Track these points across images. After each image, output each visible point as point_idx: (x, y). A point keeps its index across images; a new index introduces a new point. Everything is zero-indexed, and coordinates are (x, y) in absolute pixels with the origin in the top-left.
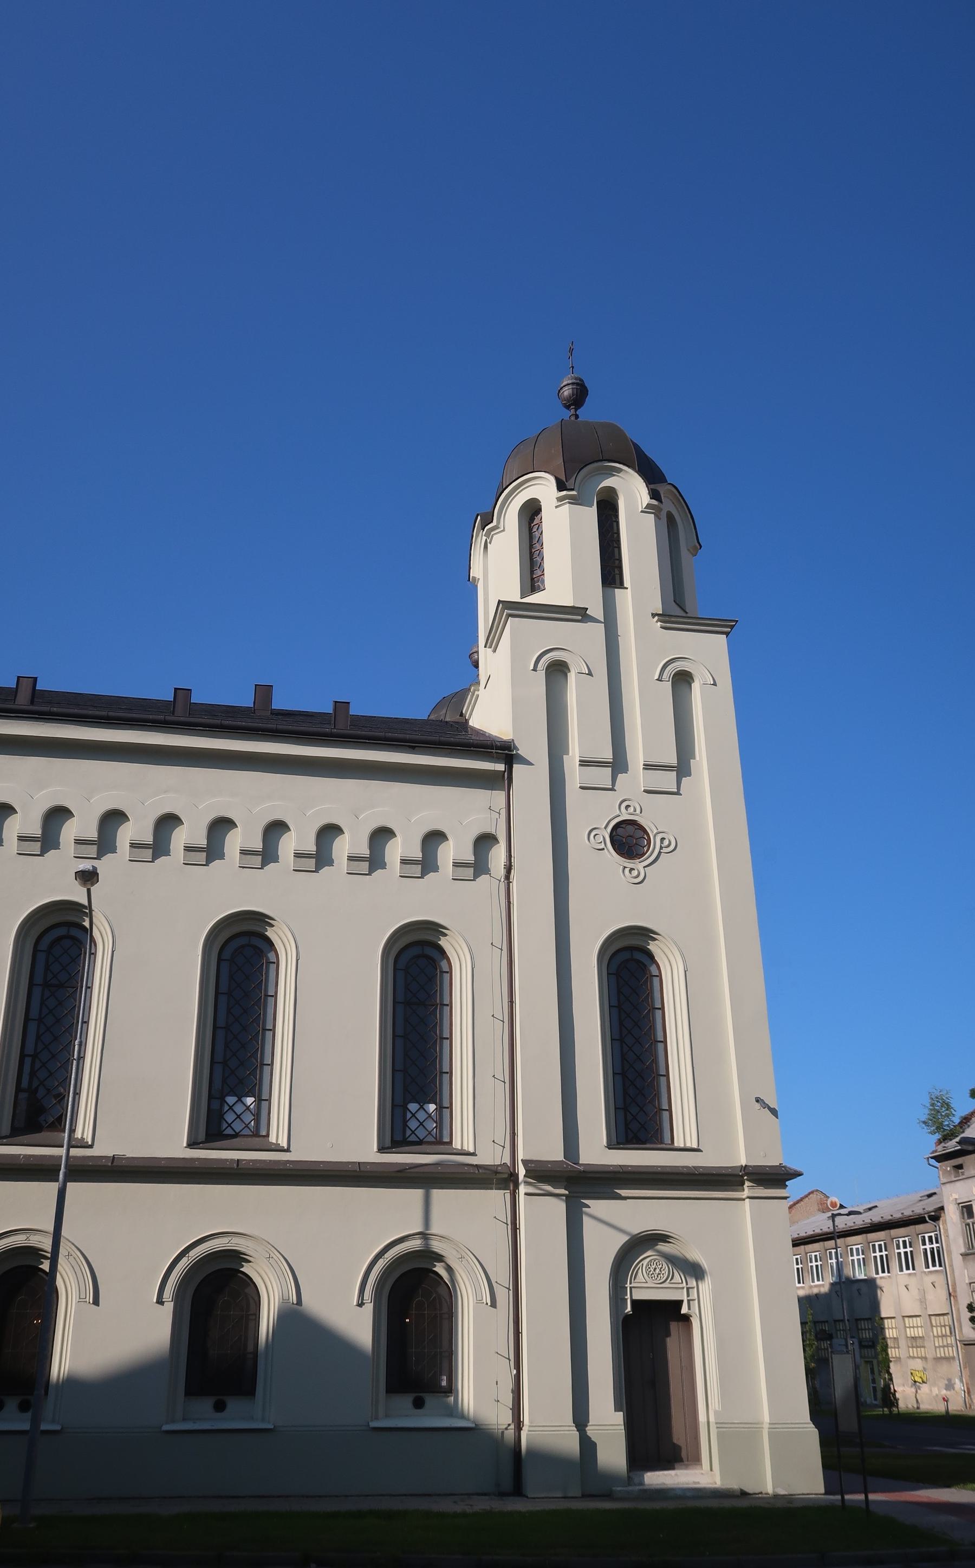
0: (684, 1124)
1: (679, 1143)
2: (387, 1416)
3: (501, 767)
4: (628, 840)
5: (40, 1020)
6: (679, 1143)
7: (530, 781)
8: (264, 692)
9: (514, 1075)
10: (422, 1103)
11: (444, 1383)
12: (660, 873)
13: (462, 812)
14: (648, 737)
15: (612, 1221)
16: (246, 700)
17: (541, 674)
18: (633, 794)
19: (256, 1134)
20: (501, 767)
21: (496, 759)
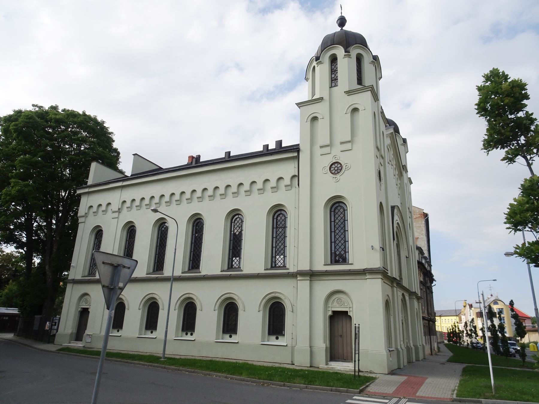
0: (351, 256)
1: (350, 263)
2: (268, 341)
3: (295, 154)
4: (336, 168)
5: (335, 242)
6: (350, 263)
7: (304, 157)
8: (279, 143)
9: (306, 246)
10: (236, 257)
11: (7, 318)
12: (343, 177)
13: (287, 170)
14: (343, 132)
15: (324, 287)
16: (261, 149)
17: (309, 123)
18: (337, 153)
19: (239, 267)
20: (295, 154)
21: (294, 152)
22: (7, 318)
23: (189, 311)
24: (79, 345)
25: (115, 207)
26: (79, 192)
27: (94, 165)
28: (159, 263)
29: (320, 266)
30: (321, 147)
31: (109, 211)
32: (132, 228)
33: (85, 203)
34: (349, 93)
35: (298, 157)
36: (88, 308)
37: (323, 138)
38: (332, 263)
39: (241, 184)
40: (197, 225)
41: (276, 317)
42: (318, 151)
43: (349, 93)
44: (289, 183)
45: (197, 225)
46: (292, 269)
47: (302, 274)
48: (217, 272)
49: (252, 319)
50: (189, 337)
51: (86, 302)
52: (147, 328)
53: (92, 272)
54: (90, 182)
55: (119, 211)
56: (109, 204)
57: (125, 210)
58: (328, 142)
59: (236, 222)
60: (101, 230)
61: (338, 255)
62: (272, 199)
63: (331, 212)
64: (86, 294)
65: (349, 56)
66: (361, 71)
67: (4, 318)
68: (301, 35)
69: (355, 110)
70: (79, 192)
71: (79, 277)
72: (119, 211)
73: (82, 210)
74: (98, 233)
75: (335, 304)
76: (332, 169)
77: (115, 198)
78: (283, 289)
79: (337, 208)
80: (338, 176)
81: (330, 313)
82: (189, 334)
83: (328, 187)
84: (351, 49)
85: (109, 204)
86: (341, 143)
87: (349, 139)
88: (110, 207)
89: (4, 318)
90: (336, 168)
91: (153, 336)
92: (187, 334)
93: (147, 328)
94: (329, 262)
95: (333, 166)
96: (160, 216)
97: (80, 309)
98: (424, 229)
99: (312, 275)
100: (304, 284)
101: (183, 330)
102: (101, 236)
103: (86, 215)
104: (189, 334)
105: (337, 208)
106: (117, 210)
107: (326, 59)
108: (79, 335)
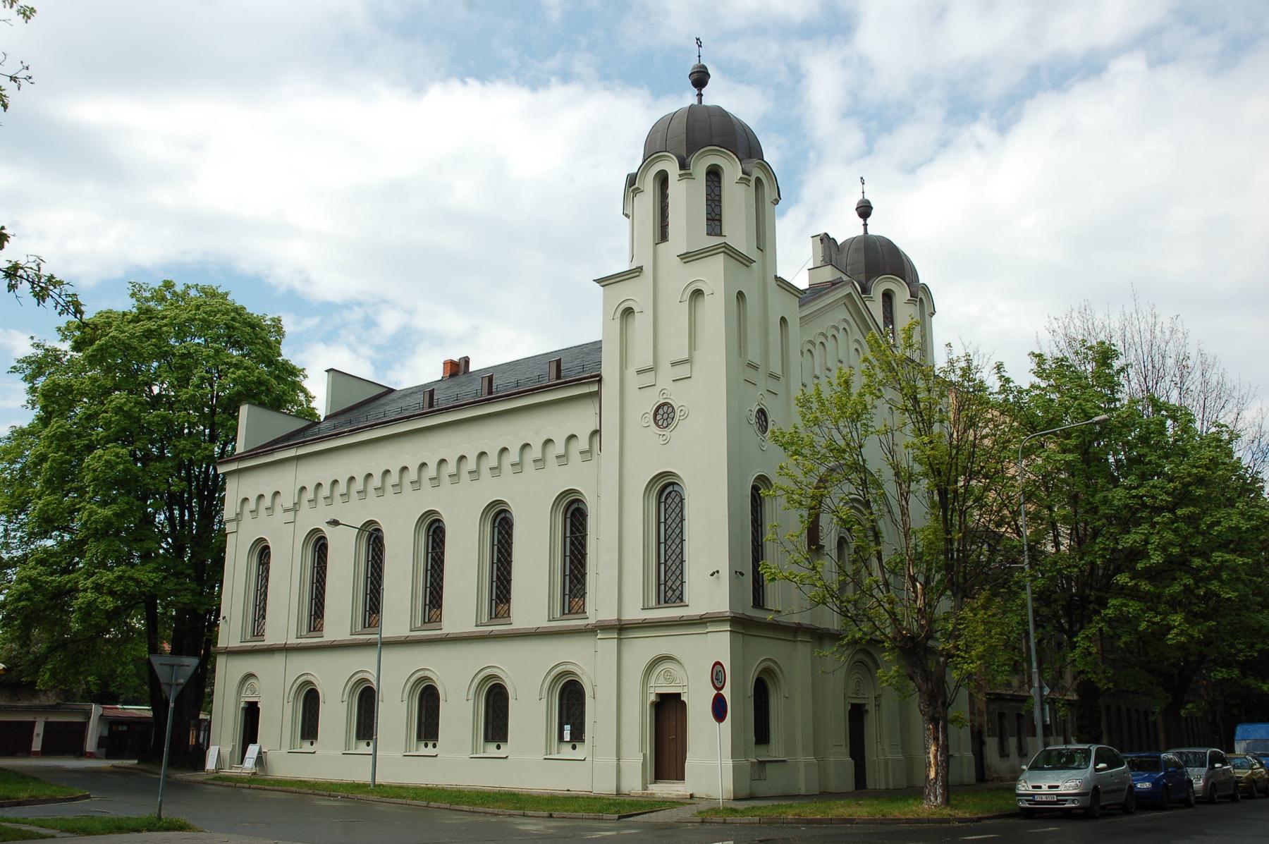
3: (595, 388)
11: (125, 728)
12: (681, 431)
13: (579, 420)
15: (642, 649)
17: (618, 321)
18: (666, 387)
20: (595, 388)
22: (125, 728)
23: (496, 702)
25: (287, 500)
26: (221, 470)
27: (244, 410)
29: (634, 612)
30: (639, 372)
31: (278, 510)
32: (575, 506)
33: (234, 492)
34: (686, 257)
35: (598, 394)
36: (679, 695)
37: (641, 355)
38: (659, 605)
39: (572, 437)
40: (501, 522)
42: (633, 381)
43: (686, 257)
44: (474, 468)
45: (501, 522)
47: (604, 627)
48: (470, 628)
50: (430, 750)
51: (670, 678)
52: (304, 737)
54: (240, 448)
55: (295, 508)
56: (277, 493)
57: (305, 504)
58: (650, 364)
59: (669, 501)
60: (267, 547)
62: (560, 480)
63: (659, 503)
64: (250, 676)
65: (689, 176)
67: (120, 728)
68: (620, 125)
69: (698, 293)
70: (221, 470)
71: (235, 643)
72: (295, 508)
73: (229, 511)
74: (263, 552)
75: (661, 680)
76: (659, 417)
77: (285, 481)
79: (666, 491)
80: (667, 432)
81: (653, 698)
82: (430, 745)
83: (651, 455)
84: (692, 160)
85: (277, 493)
86: (673, 364)
87: (686, 356)
88: (279, 500)
89: (120, 728)
90: (664, 414)
91: (311, 749)
92: (426, 746)
93: (304, 737)
94: (653, 602)
95: (661, 411)
97: (242, 705)
99: (621, 629)
100: (607, 646)
101: (419, 738)
103: (238, 518)
104: (430, 745)
105: (666, 491)
106: (291, 506)
107: (649, 184)
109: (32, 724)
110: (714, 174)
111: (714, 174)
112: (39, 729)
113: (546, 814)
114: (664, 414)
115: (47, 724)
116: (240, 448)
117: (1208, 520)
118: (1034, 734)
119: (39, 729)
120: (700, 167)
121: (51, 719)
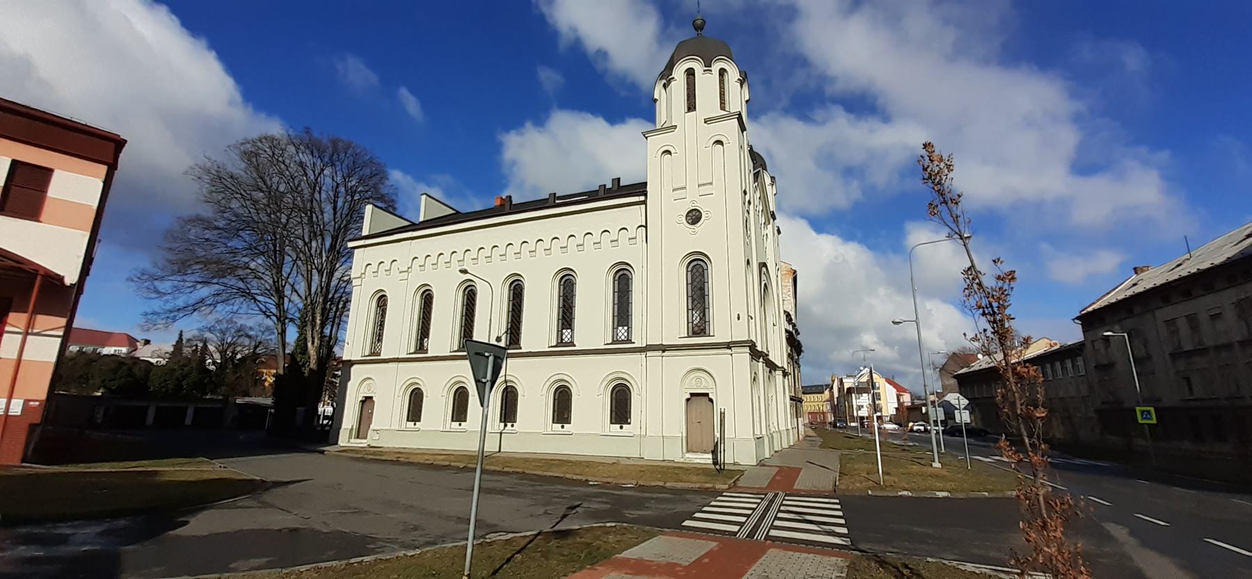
3: (642, 198)
9: (661, 309)
13: (633, 216)
20: (642, 198)
24: (362, 443)
26: (350, 245)
27: (369, 208)
28: (566, 318)
35: (644, 202)
41: (621, 407)
46: (638, 344)
49: (591, 406)
53: (422, 344)
54: (365, 232)
61: (700, 328)
66: (702, 289)
74: (382, 302)
78: (628, 367)
79: (697, 269)
90: (694, 217)
96: (467, 276)
98: (792, 289)
102: (431, 303)
105: (697, 269)
108: (360, 432)
109: (147, 408)
110: (722, 72)
111: (722, 72)
112: (190, 412)
113: (542, 511)
114: (694, 217)
115: (158, 409)
116: (365, 232)
117: (235, 243)
118: (155, 473)
119: (190, 412)
120: (716, 67)
121: (162, 404)
